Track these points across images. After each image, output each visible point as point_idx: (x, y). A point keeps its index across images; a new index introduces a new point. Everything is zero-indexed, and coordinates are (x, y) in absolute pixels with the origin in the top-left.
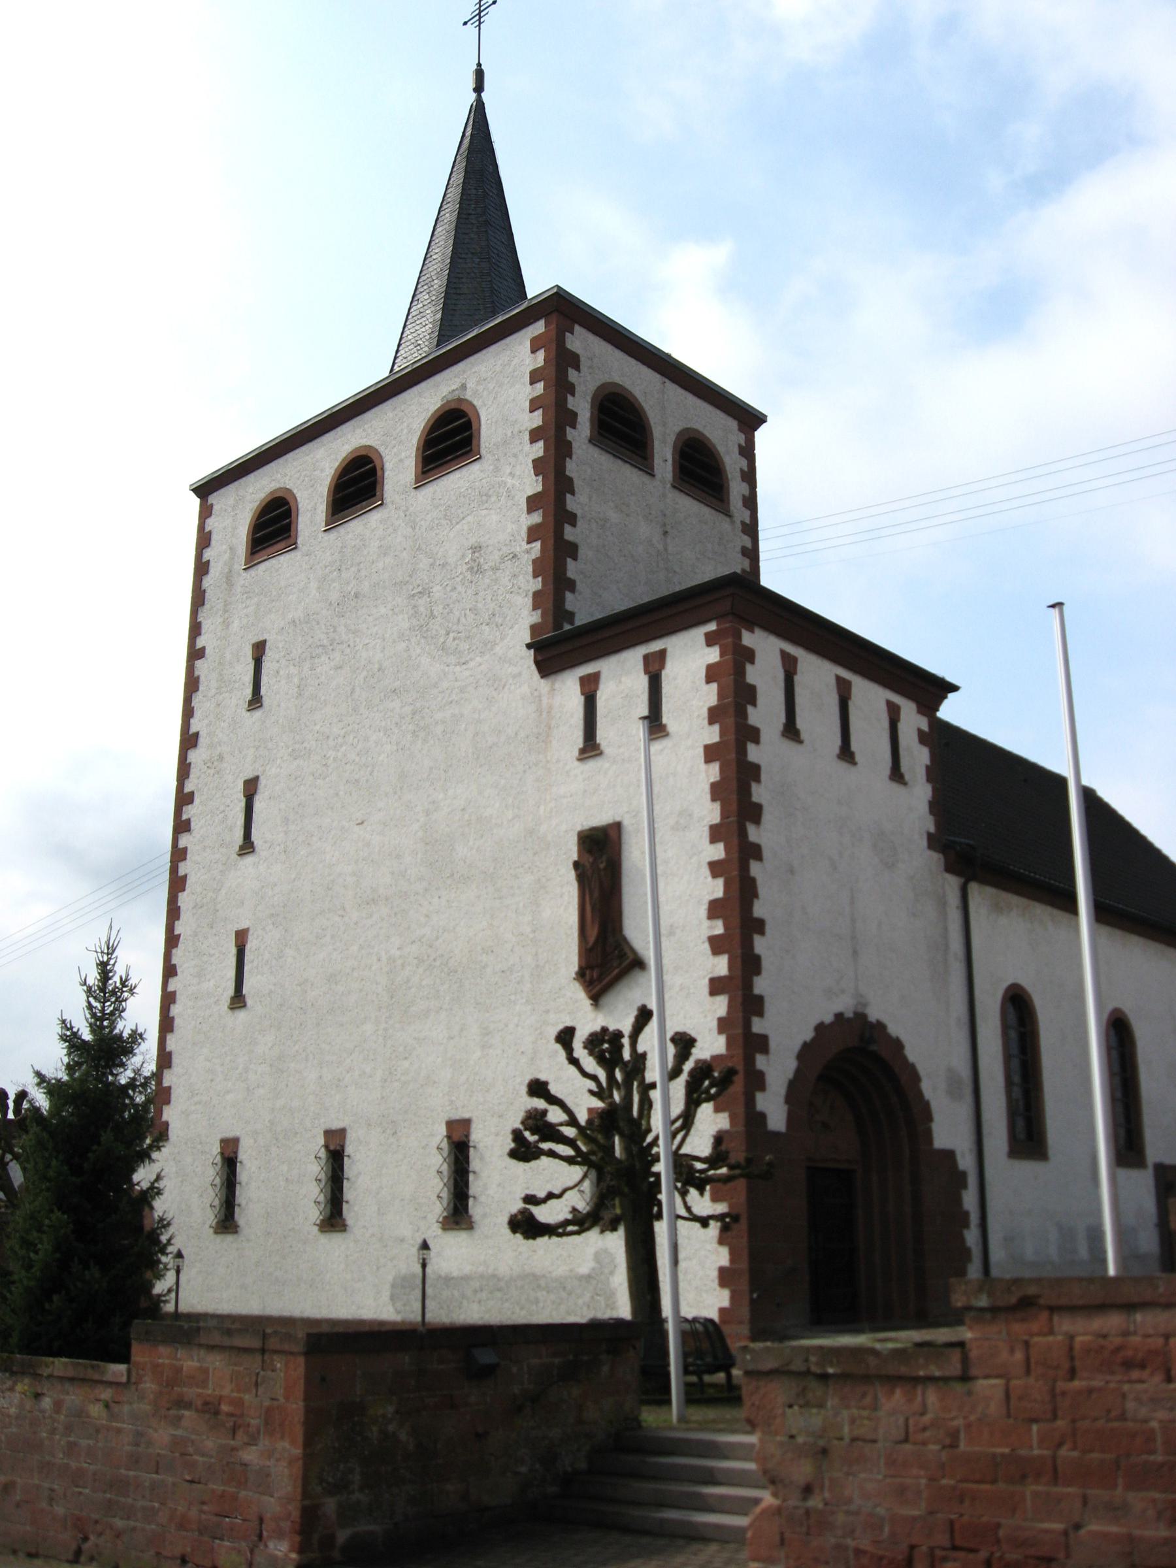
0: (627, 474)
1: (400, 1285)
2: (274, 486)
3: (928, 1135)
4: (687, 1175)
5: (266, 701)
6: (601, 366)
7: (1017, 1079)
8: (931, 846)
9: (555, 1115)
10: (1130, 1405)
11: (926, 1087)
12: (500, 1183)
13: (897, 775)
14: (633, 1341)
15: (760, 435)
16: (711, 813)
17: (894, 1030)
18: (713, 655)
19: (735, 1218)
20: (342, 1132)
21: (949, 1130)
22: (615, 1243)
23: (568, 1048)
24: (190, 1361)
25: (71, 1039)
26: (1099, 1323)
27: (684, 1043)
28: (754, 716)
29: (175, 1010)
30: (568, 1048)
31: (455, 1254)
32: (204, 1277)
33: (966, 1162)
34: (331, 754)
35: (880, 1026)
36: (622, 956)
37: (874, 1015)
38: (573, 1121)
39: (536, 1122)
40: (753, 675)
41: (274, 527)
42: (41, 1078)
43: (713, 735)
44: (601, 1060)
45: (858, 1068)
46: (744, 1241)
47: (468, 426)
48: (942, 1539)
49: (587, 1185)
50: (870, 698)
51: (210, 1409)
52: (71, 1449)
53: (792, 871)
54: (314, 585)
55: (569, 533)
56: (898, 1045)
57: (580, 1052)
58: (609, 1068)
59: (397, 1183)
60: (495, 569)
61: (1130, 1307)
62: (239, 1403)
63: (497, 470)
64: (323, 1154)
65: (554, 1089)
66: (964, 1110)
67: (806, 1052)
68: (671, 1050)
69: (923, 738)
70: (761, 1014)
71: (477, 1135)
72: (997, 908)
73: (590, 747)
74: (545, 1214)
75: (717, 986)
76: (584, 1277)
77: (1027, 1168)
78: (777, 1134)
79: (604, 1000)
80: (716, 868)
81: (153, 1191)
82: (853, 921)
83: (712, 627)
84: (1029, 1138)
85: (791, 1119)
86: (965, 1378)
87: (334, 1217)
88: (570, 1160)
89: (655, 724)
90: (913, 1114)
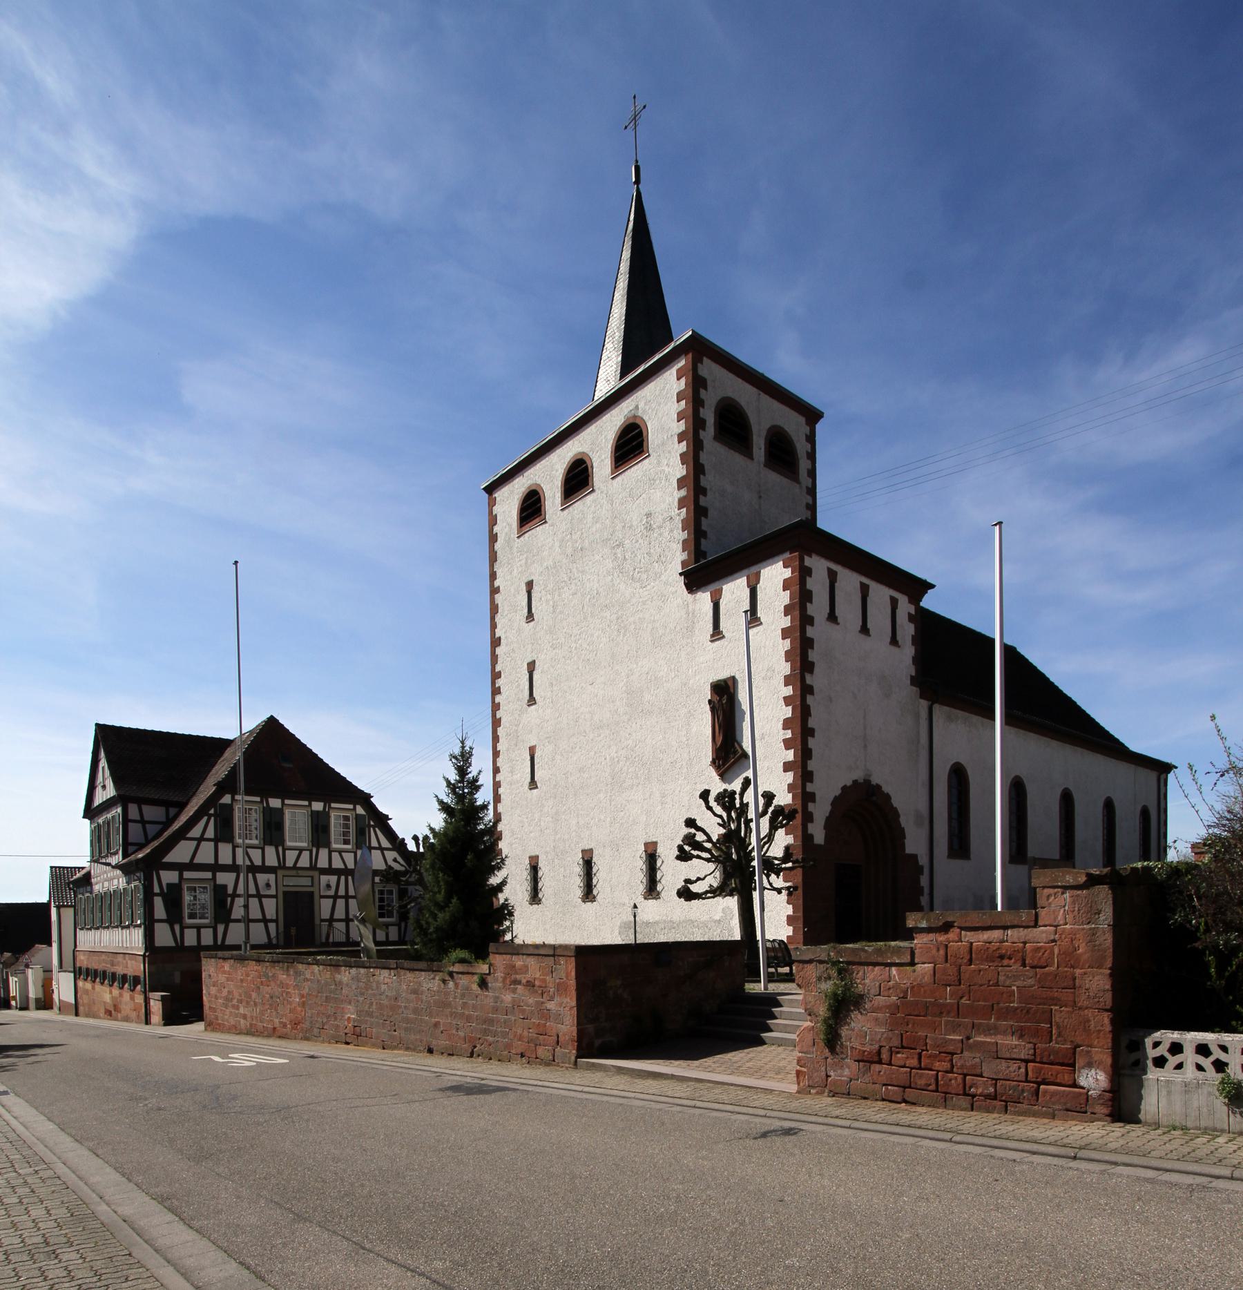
0: (738, 459)
1: (624, 926)
2: (530, 482)
3: (903, 846)
4: (769, 866)
5: (536, 617)
6: (723, 384)
7: (955, 815)
8: (912, 684)
9: (700, 837)
10: (1002, 978)
11: (903, 821)
12: (673, 873)
13: (894, 641)
14: (740, 954)
15: (819, 427)
16: (786, 668)
17: (886, 789)
18: (788, 573)
19: (795, 888)
20: (591, 851)
21: (915, 843)
22: (732, 903)
23: (707, 802)
24: (519, 962)
25: (444, 807)
26: (986, 935)
27: (769, 797)
28: (811, 609)
29: (501, 791)
30: (707, 802)
31: (650, 910)
32: (528, 927)
33: (923, 861)
34: (574, 645)
35: (879, 787)
36: (735, 752)
37: (875, 780)
38: (709, 840)
39: (689, 839)
40: (811, 584)
41: (531, 509)
42: (432, 830)
43: (786, 622)
44: (724, 808)
45: (864, 809)
46: (801, 902)
47: (640, 434)
48: (896, 1042)
49: (717, 874)
50: (880, 594)
51: (530, 984)
52: (465, 1005)
53: (831, 700)
54: (557, 544)
55: (703, 501)
56: (888, 797)
57: (713, 803)
58: (728, 811)
59: (620, 876)
60: (660, 527)
61: (1005, 928)
62: (544, 981)
63: (659, 463)
64: (581, 862)
65: (699, 823)
66: (924, 832)
67: (836, 802)
68: (761, 801)
69: (911, 618)
70: (811, 781)
71: (660, 850)
72: (949, 719)
73: (717, 633)
74: (695, 888)
75: (787, 767)
76: (717, 920)
77: (958, 863)
78: (820, 846)
79: (726, 776)
80: (788, 701)
81: (499, 888)
82: (865, 728)
83: (787, 555)
84: (960, 845)
85: (828, 838)
86: (912, 964)
87: (589, 893)
88: (708, 860)
89: (753, 618)
90: (898, 835)
